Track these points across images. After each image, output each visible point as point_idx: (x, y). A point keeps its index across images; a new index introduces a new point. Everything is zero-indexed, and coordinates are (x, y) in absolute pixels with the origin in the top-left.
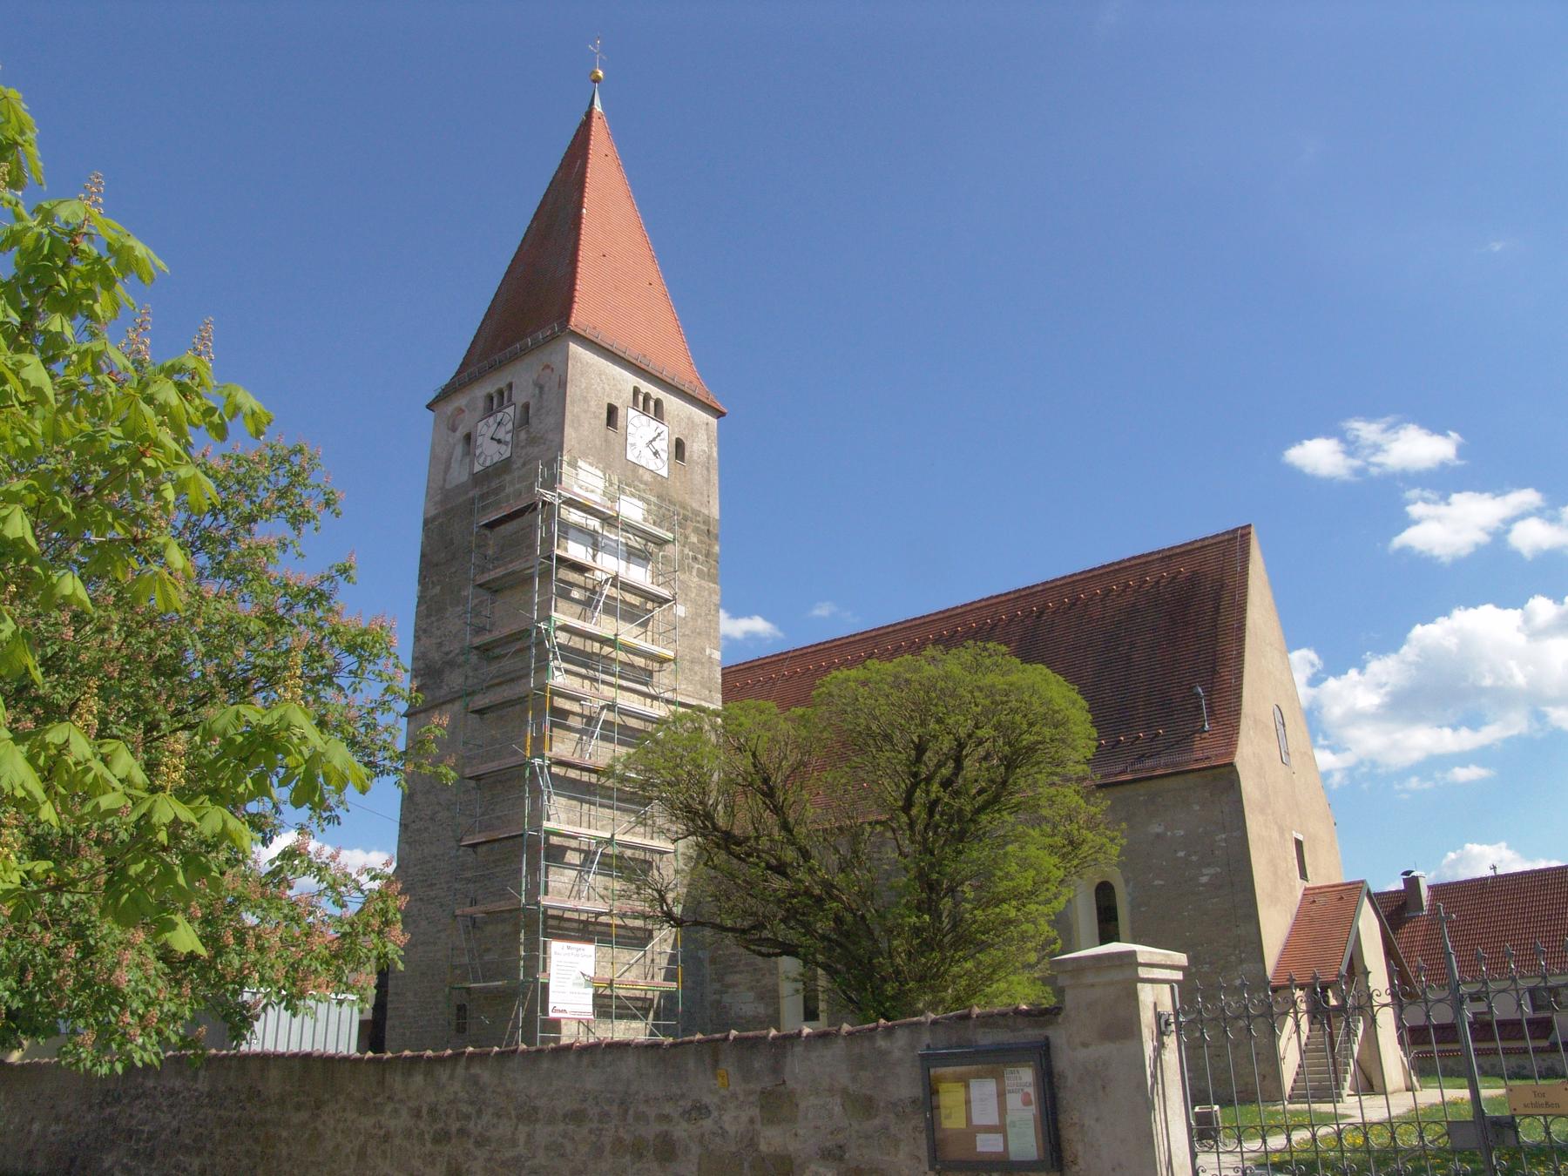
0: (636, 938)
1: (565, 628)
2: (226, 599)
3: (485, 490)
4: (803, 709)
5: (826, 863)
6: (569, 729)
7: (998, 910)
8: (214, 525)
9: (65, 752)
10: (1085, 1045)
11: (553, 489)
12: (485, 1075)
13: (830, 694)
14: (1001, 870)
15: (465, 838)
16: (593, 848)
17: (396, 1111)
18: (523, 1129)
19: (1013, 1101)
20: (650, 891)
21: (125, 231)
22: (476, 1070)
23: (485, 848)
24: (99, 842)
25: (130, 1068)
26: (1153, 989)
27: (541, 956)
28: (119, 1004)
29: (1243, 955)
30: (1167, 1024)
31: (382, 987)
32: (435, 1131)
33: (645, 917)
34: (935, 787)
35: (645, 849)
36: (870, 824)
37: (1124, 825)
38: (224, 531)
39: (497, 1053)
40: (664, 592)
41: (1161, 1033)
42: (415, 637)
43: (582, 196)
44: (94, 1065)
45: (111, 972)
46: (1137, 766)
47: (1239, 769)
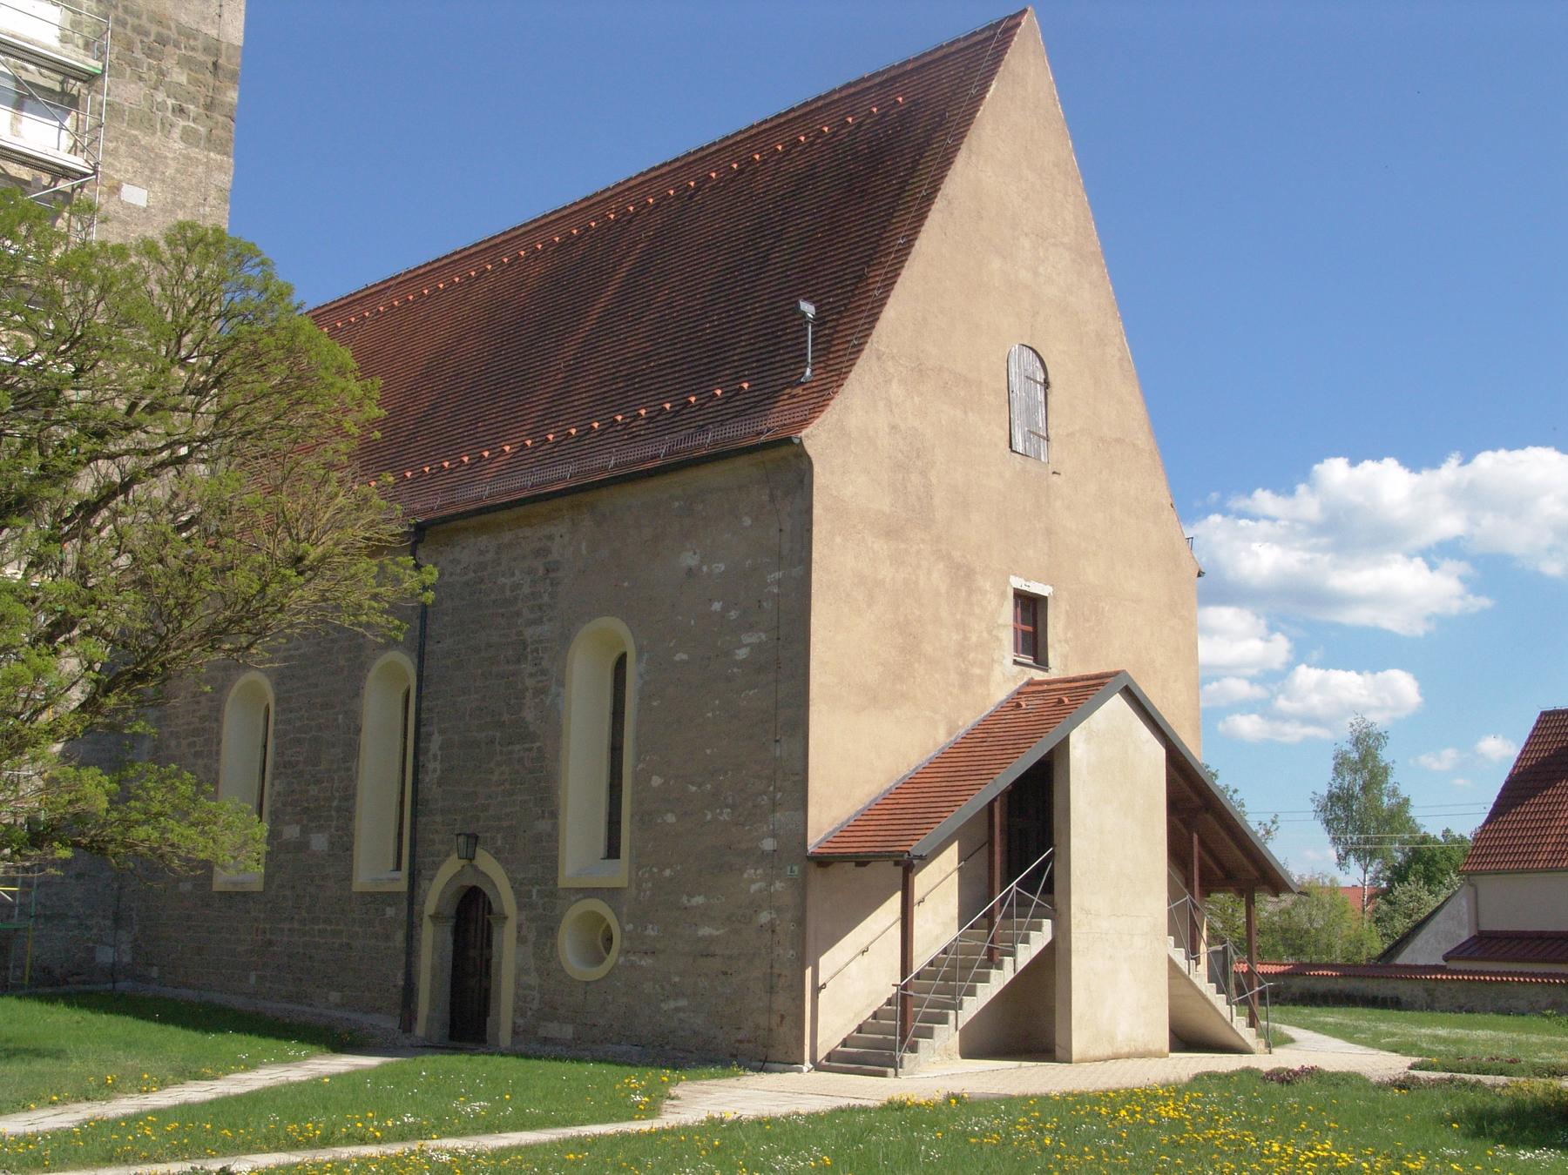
29: (779, 795)
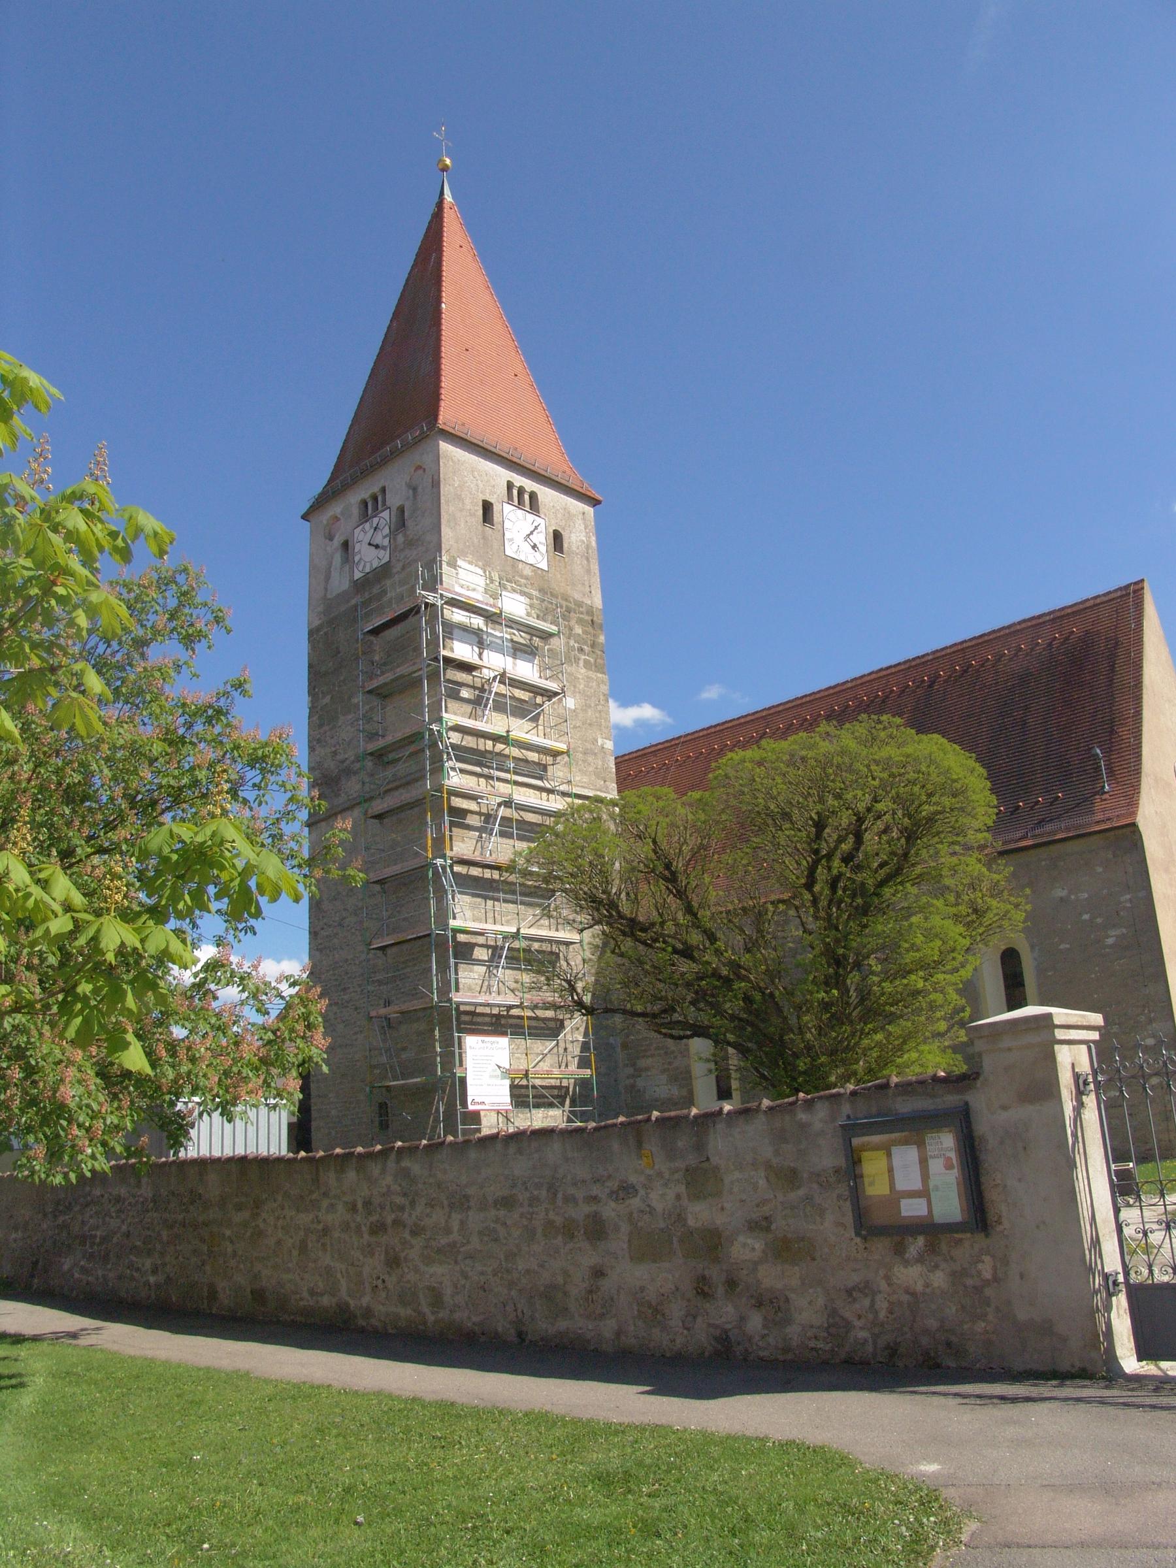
0: (549, 1029)
1: (457, 728)
2: (127, 723)
3: (367, 595)
4: (700, 793)
5: (732, 944)
6: (469, 827)
7: (905, 981)
8: (109, 651)
9: (5, 880)
10: (1005, 1108)
11: (435, 590)
12: (415, 1167)
13: (727, 776)
14: (906, 941)
15: (374, 941)
16: (499, 943)
17: (332, 1205)
18: (456, 1217)
19: (936, 1166)
20: (559, 981)
21: (16, 361)
22: (406, 1163)
23: (394, 950)
24: (29, 967)
25: (81, 1177)
26: (1070, 1050)
27: (457, 1051)
28: (65, 1119)
30: (1086, 1083)
31: (304, 1089)
32: (372, 1223)
33: (555, 1007)
34: (836, 863)
35: (550, 941)
36: (772, 903)
37: (1028, 891)
38: (119, 657)
39: (425, 1146)
40: (553, 686)
41: (1080, 1093)
42: (310, 747)
43: (440, 291)
44: (48, 1176)
45: (55, 1091)
46: (1037, 832)
47: (1141, 829)
